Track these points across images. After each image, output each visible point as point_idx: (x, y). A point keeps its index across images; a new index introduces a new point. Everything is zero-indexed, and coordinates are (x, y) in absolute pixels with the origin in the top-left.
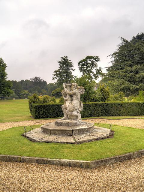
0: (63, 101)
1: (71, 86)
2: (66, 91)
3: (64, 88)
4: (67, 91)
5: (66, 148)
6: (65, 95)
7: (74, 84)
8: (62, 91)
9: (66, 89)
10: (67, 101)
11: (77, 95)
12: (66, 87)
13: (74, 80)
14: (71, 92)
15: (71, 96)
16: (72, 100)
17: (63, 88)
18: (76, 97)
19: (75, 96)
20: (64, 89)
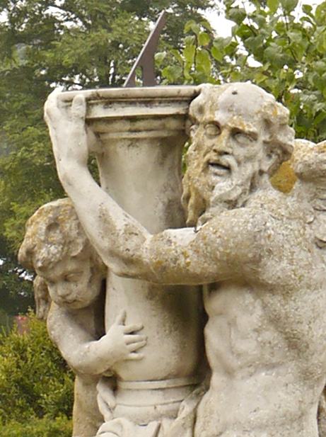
0: (47, 399)
1: (172, 141)
2: (93, 228)
3: (69, 168)
4: (120, 219)
5: (216, 174)
6: (82, 290)
7: (237, 98)
8: (36, 226)
9: (85, 193)
10: (113, 381)
11: (284, 289)
12: (96, 163)
13: (223, 28)
14: (183, 236)
15: (185, 303)
16: (197, 375)
17: (44, 181)
18: (275, 321)
19: (248, 298)
20: (60, 192)
